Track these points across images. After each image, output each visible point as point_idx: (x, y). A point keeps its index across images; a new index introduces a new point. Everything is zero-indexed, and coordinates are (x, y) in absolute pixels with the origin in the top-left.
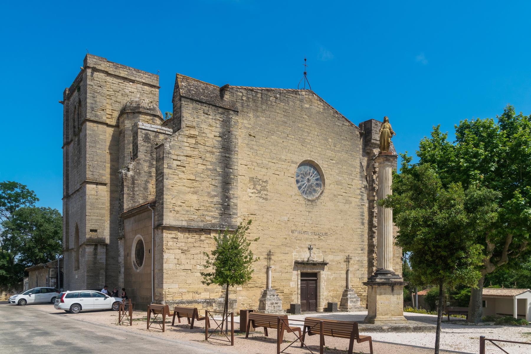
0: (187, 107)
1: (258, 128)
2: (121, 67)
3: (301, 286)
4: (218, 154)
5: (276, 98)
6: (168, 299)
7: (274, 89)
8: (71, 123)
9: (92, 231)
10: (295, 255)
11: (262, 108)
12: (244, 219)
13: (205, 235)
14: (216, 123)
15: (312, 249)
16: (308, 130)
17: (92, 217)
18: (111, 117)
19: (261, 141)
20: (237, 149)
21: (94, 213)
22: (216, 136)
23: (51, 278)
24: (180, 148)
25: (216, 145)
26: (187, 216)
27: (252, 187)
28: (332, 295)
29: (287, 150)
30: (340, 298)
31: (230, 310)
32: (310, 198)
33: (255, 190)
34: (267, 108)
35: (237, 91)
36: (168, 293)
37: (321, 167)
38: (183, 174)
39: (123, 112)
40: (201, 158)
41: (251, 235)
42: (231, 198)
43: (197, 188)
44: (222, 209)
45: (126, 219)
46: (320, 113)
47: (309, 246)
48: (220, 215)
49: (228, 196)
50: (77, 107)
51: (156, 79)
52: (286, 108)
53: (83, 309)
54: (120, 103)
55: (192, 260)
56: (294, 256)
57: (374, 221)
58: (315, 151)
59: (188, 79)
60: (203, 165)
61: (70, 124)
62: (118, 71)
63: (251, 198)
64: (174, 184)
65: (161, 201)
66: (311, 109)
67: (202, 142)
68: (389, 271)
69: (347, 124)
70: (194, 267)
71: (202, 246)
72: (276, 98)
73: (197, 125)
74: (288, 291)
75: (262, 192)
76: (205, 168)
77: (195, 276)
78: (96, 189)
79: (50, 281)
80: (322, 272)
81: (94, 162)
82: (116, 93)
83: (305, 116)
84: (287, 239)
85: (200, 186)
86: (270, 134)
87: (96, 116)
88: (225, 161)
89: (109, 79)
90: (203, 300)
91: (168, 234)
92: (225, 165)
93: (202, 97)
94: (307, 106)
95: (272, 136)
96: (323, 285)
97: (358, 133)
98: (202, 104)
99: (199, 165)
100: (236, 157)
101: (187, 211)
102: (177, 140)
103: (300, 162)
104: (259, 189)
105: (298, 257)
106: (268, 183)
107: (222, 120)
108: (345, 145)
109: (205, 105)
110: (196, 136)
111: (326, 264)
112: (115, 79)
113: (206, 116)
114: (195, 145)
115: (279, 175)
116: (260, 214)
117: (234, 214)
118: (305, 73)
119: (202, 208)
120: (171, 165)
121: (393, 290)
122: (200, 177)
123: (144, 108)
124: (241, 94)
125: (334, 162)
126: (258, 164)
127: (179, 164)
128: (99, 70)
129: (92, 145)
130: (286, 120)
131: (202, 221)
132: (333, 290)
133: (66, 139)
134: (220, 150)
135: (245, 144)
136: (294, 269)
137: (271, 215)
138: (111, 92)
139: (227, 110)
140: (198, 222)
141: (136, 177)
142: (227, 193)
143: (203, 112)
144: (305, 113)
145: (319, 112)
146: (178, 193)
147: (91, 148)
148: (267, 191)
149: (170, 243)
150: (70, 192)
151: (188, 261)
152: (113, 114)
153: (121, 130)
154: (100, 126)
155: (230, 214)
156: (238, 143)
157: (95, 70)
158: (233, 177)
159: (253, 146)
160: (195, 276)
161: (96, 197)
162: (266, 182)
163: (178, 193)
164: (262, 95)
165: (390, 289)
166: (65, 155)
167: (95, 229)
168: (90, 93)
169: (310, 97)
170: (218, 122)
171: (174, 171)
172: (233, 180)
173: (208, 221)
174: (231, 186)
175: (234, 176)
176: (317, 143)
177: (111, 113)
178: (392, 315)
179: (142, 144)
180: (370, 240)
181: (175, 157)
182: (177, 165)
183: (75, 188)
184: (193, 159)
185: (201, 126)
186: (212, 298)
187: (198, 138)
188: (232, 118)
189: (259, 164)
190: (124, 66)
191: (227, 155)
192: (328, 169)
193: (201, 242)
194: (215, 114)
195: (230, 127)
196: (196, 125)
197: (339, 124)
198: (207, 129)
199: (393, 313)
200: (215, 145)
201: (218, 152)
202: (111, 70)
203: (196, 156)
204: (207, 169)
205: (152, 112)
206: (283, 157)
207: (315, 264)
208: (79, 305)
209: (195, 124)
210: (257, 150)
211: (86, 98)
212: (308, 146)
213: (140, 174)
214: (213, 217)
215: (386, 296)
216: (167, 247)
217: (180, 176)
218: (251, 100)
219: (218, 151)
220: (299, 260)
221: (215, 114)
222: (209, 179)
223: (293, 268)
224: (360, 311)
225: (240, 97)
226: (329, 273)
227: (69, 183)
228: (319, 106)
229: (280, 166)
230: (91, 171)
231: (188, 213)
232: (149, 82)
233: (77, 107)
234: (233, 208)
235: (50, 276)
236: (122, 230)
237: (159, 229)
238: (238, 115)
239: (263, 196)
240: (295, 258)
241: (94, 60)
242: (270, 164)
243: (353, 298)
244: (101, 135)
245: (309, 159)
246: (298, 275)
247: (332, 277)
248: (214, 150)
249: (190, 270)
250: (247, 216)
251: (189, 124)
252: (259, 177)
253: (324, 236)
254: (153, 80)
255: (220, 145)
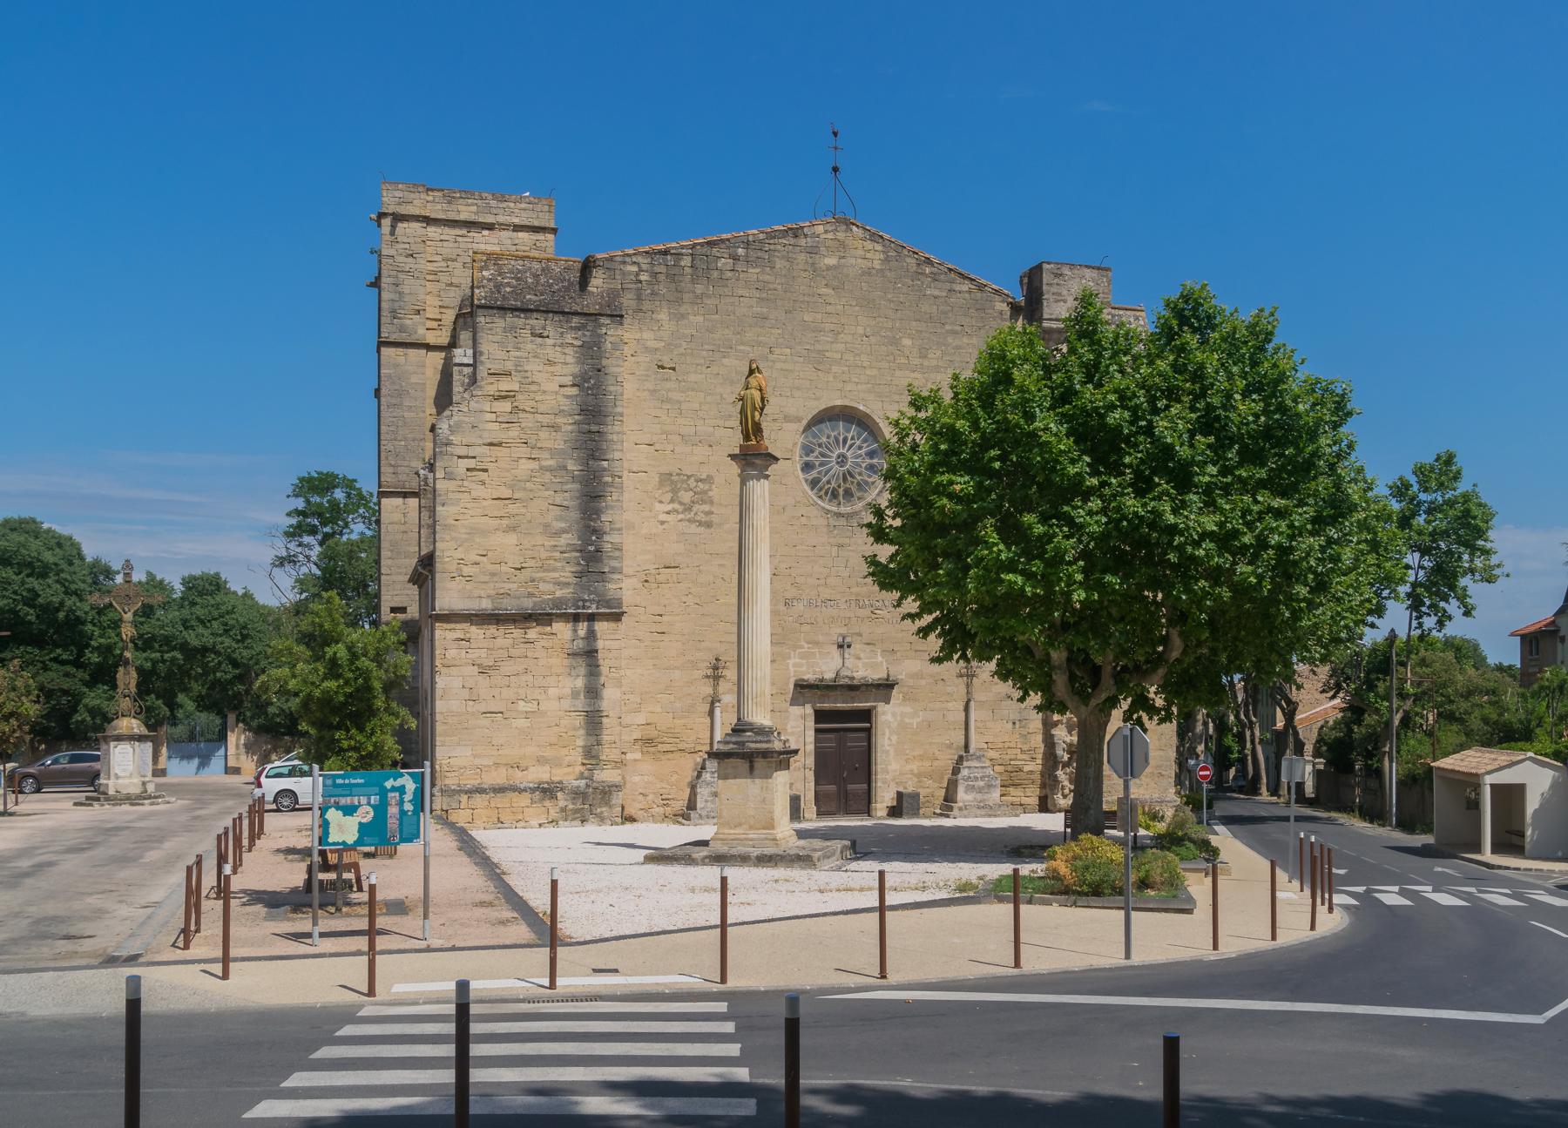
0: (490, 329)
2: (461, 198)
3: (816, 748)
4: (570, 428)
5: (735, 258)
6: (447, 782)
7: (729, 236)
9: (393, 610)
10: (795, 665)
11: (694, 292)
13: (539, 629)
14: (565, 354)
15: (849, 646)
17: (394, 578)
19: (693, 377)
20: (619, 410)
21: (399, 567)
24: (473, 427)
26: (492, 585)
28: (916, 771)
30: (942, 778)
31: (604, 809)
32: (843, 509)
33: (676, 506)
35: (624, 263)
38: (483, 487)
42: (605, 533)
43: (517, 518)
46: (874, 272)
47: (840, 640)
49: (598, 528)
51: (546, 208)
52: (767, 278)
53: (300, 801)
55: (505, 691)
58: (857, 380)
59: (500, 259)
63: (665, 526)
67: (527, 405)
68: (751, 724)
69: (966, 286)
70: (510, 705)
72: (735, 258)
73: (516, 366)
76: (537, 467)
77: (514, 726)
78: (404, 507)
80: (881, 707)
81: (397, 443)
83: (824, 290)
85: (524, 511)
87: (402, 329)
88: (591, 445)
89: (433, 231)
90: (531, 785)
92: (590, 453)
93: (528, 297)
96: (887, 742)
98: (528, 315)
100: (616, 428)
101: (493, 574)
102: (466, 409)
103: (810, 417)
105: (804, 669)
107: (580, 343)
108: (958, 347)
109: (535, 315)
110: (513, 393)
112: (447, 230)
113: (539, 340)
117: (613, 571)
118: (835, 170)
119: (531, 563)
121: (752, 768)
122: (525, 489)
124: (635, 269)
130: (765, 310)
131: (530, 595)
132: (922, 758)
134: (576, 417)
136: (794, 702)
138: (439, 264)
139: (593, 318)
140: (519, 598)
142: (594, 520)
144: (824, 282)
145: (868, 272)
146: (469, 534)
148: (712, 503)
149: (452, 653)
151: (496, 692)
152: (444, 316)
154: (411, 352)
156: (622, 395)
157: (398, 218)
159: (669, 394)
160: (514, 726)
161: (402, 528)
162: (709, 479)
163: (469, 534)
165: (747, 765)
169: (841, 235)
170: (569, 350)
171: (460, 483)
173: (544, 593)
175: (613, 476)
176: (864, 357)
177: (439, 317)
178: (751, 828)
181: (463, 451)
186: (556, 779)
187: (519, 397)
189: (686, 438)
190: (467, 193)
191: (594, 428)
193: (528, 645)
194: (562, 333)
195: (600, 358)
197: (936, 293)
199: (752, 823)
200: (562, 408)
201: (570, 424)
202: (436, 211)
204: (541, 468)
207: (853, 688)
208: (291, 793)
209: (509, 366)
210: (680, 403)
212: (835, 369)
214: (559, 584)
215: (738, 781)
216: (445, 661)
217: (474, 494)
218: (662, 277)
219: (571, 421)
220: (810, 677)
222: (548, 493)
223: (789, 700)
224: (990, 816)
225: (632, 277)
226: (908, 709)
231: (495, 579)
238: (621, 324)
240: (795, 672)
241: (398, 194)
243: (976, 778)
244: (415, 373)
245: (838, 403)
246: (804, 717)
247: (915, 722)
248: (560, 420)
249: (502, 713)
250: (654, 572)
251: (495, 367)
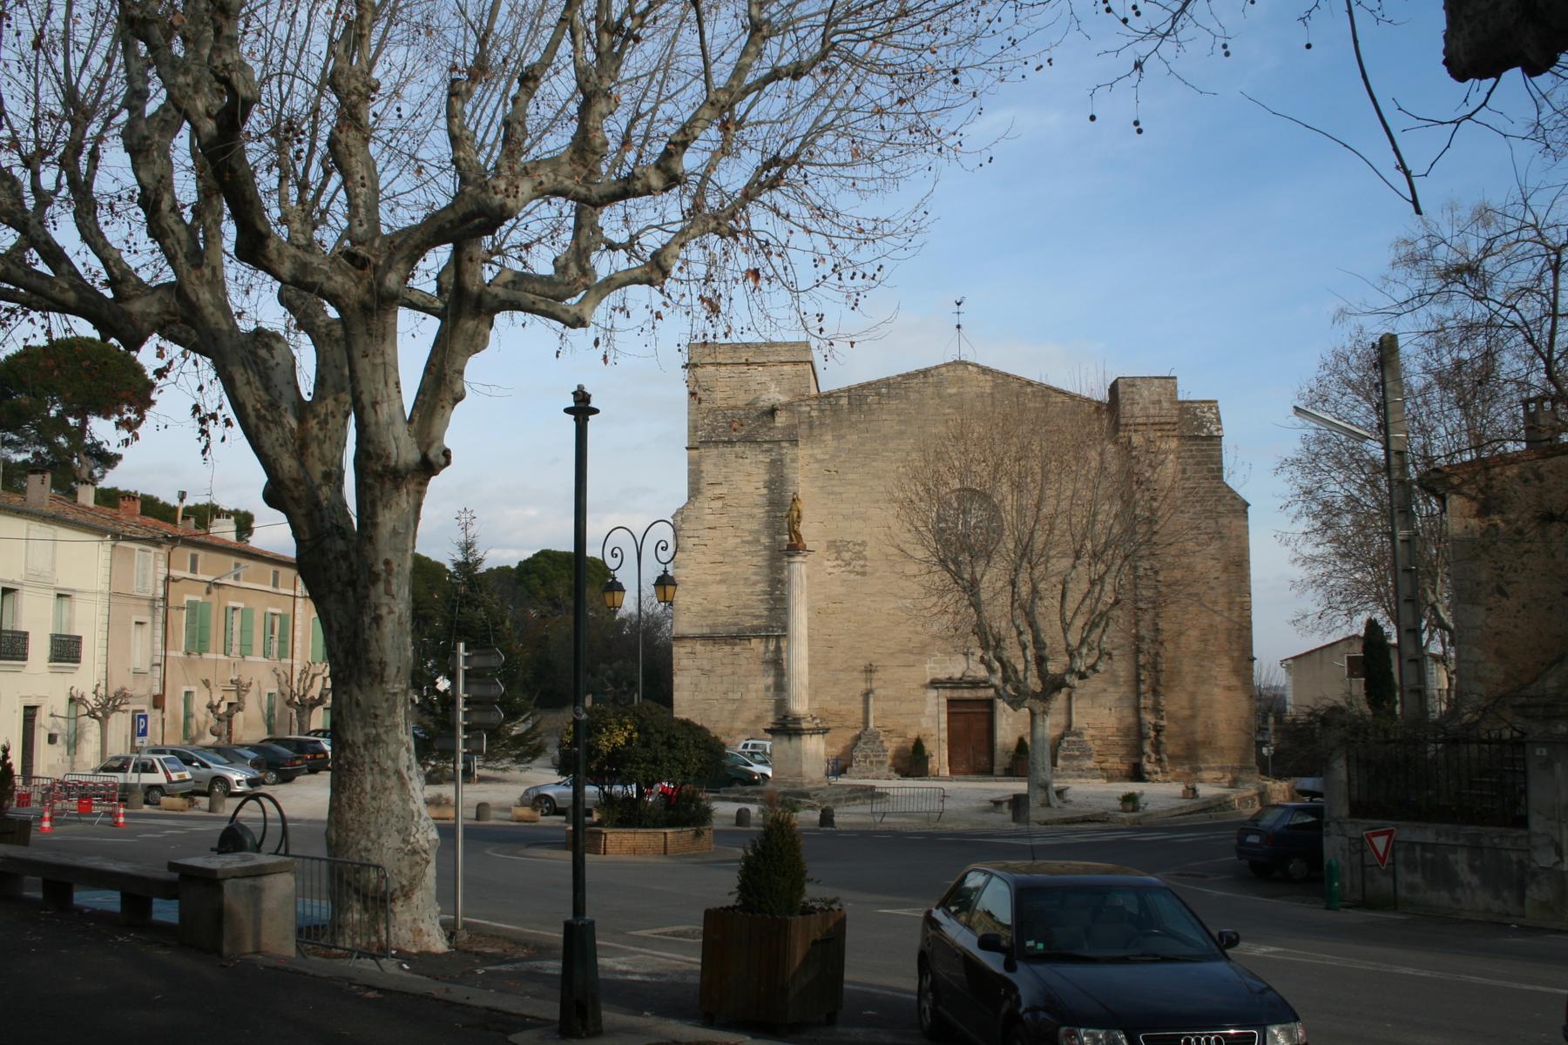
33: (839, 562)
124: (808, 409)
181: (690, 533)
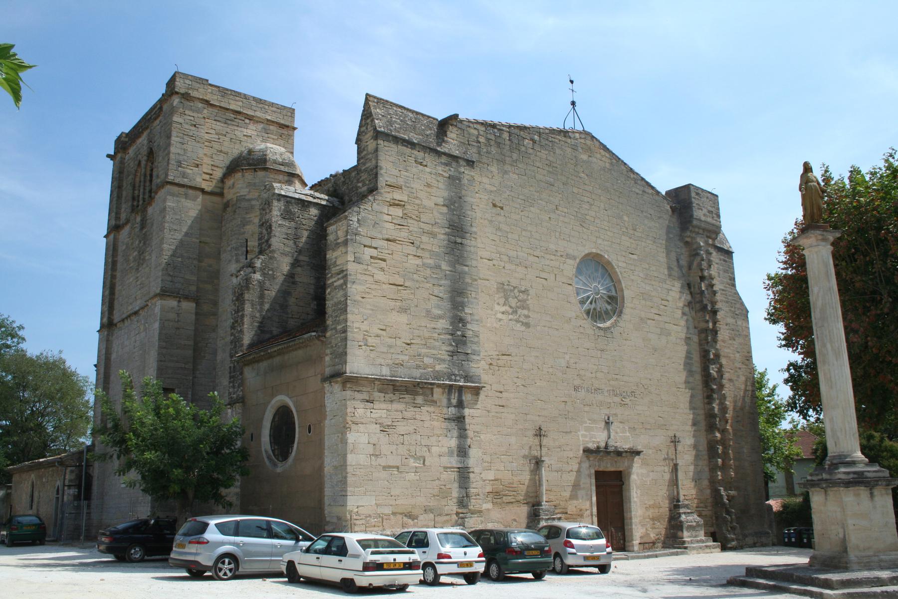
0: (387, 151)
1: (508, 192)
2: (231, 94)
5: (534, 142)
8: (127, 192)
11: (511, 157)
12: (491, 364)
14: (438, 181)
15: (612, 423)
16: (589, 200)
18: (210, 178)
20: (474, 229)
22: (438, 205)
23: (69, 486)
25: (439, 221)
27: (502, 301)
29: (557, 234)
33: (507, 308)
34: (520, 158)
35: (469, 127)
36: (355, 517)
37: (616, 267)
38: (383, 273)
39: (234, 167)
40: (413, 243)
41: (504, 395)
43: (407, 302)
44: (453, 344)
45: (248, 365)
48: (449, 355)
50: (143, 163)
52: (551, 159)
54: (226, 153)
56: (581, 439)
57: (711, 369)
58: (603, 237)
60: (416, 258)
61: (124, 193)
62: (226, 100)
64: (365, 293)
65: (339, 327)
66: (591, 162)
70: (404, 460)
71: (418, 417)
72: (534, 142)
74: (575, 509)
75: (520, 311)
76: (421, 263)
79: (66, 493)
82: (220, 136)
84: (568, 404)
85: (412, 296)
86: (527, 204)
87: (184, 175)
91: (356, 393)
94: (584, 157)
95: (532, 209)
97: (668, 207)
99: (410, 257)
100: (473, 243)
101: (390, 347)
102: (370, 209)
103: (580, 257)
104: (513, 305)
106: (528, 295)
108: (650, 228)
111: (638, 453)
113: (421, 167)
114: (403, 220)
115: (546, 279)
116: (518, 355)
118: (573, 103)
120: (361, 256)
123: (275, 162)
124: (476, 132)
125: (635, 257)
126: (509, 257)
127: (375, 255)
128: (195, 98)
129: (175, 227)
131: (418, 367)
133: (116, 220)
134: (447, 230)
135: (486, 221)
137: (537, 357)
141: (267, 283)
143: (415, 161)
146: (372, 310)
147: (172, 233)
148: (529, 309)
150: (116, 318)
153: (228, 201)
155: (468, 354)
158: (470, 281)
162: (525, 292)
163: (372, 310)
164: (510, 136)
166: (111, 248)
167: (171, 387)
168: (177, 137)
171: (366, 267)
172: (470, 286)
174: (468, 298)
176: (606, 223)
177: (211, 172)
179: (280, 222)
180: (706, 405)
181: (367, 242)
182: (371, 257)
183: (130, 308)
184: (400, 246)
185: (412, 186)
187: (407, 207)
188: (464, 172)
189: (512, 259)
191: (459, 240)
192: (627, 270)
196: (404, 184)
197: (637, 191)
198: (421, 190)
203: (405, 240)
204: (424, 265)
205: (286, 169)
206: (552, 247)
209: (401, 182)
210: (507, 233)
211: (169, 145)
212: (591, 228)
213: (274, 278)
216: (354, 419)
218: (492, 143)
219: (443, 232)
220: (592, 446)
221: (436, 165)
227: (114, 301)
228: (603, 159)
229: (547, 262)
230: (169, 275)
232: (278, 119)
233: (143, 163)
234: (472, 342)
235: (67, 483)
236: (239, 387)
237: (337, 382)
239: (521, 319)
242: (531, 258)
245: (594, 251)
249: (398, 468)
251: (391, 181)
252: (514, 282)
253: (631, 398)
254: (285, 117)
255: (445, 221)
